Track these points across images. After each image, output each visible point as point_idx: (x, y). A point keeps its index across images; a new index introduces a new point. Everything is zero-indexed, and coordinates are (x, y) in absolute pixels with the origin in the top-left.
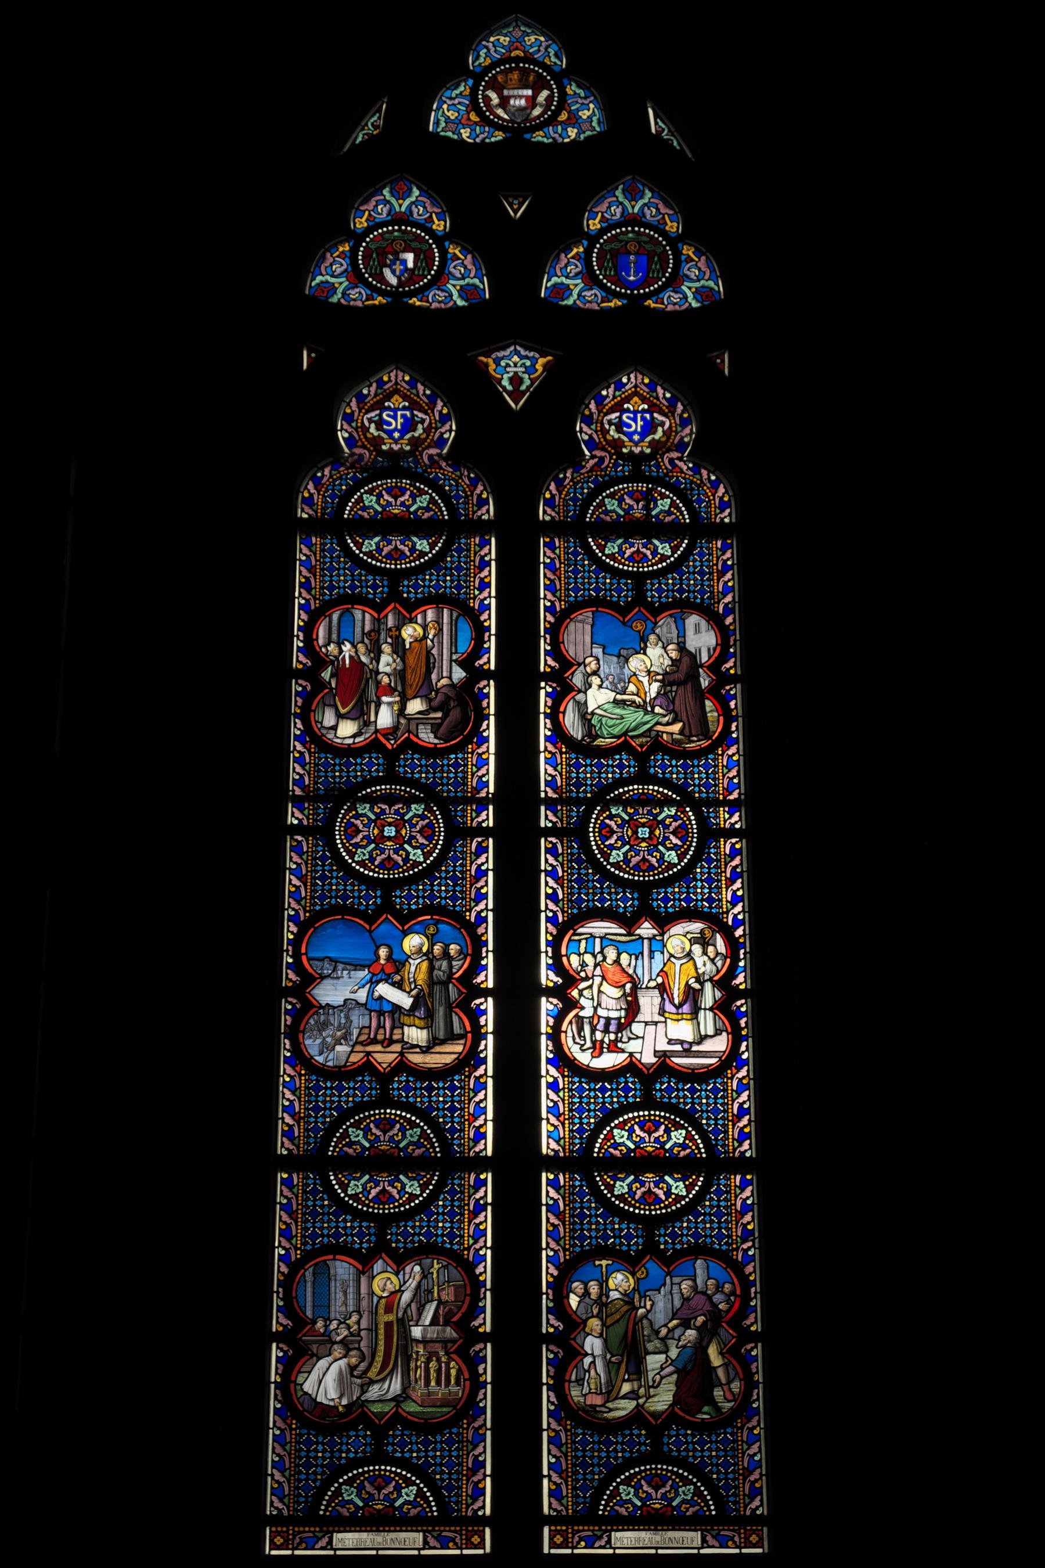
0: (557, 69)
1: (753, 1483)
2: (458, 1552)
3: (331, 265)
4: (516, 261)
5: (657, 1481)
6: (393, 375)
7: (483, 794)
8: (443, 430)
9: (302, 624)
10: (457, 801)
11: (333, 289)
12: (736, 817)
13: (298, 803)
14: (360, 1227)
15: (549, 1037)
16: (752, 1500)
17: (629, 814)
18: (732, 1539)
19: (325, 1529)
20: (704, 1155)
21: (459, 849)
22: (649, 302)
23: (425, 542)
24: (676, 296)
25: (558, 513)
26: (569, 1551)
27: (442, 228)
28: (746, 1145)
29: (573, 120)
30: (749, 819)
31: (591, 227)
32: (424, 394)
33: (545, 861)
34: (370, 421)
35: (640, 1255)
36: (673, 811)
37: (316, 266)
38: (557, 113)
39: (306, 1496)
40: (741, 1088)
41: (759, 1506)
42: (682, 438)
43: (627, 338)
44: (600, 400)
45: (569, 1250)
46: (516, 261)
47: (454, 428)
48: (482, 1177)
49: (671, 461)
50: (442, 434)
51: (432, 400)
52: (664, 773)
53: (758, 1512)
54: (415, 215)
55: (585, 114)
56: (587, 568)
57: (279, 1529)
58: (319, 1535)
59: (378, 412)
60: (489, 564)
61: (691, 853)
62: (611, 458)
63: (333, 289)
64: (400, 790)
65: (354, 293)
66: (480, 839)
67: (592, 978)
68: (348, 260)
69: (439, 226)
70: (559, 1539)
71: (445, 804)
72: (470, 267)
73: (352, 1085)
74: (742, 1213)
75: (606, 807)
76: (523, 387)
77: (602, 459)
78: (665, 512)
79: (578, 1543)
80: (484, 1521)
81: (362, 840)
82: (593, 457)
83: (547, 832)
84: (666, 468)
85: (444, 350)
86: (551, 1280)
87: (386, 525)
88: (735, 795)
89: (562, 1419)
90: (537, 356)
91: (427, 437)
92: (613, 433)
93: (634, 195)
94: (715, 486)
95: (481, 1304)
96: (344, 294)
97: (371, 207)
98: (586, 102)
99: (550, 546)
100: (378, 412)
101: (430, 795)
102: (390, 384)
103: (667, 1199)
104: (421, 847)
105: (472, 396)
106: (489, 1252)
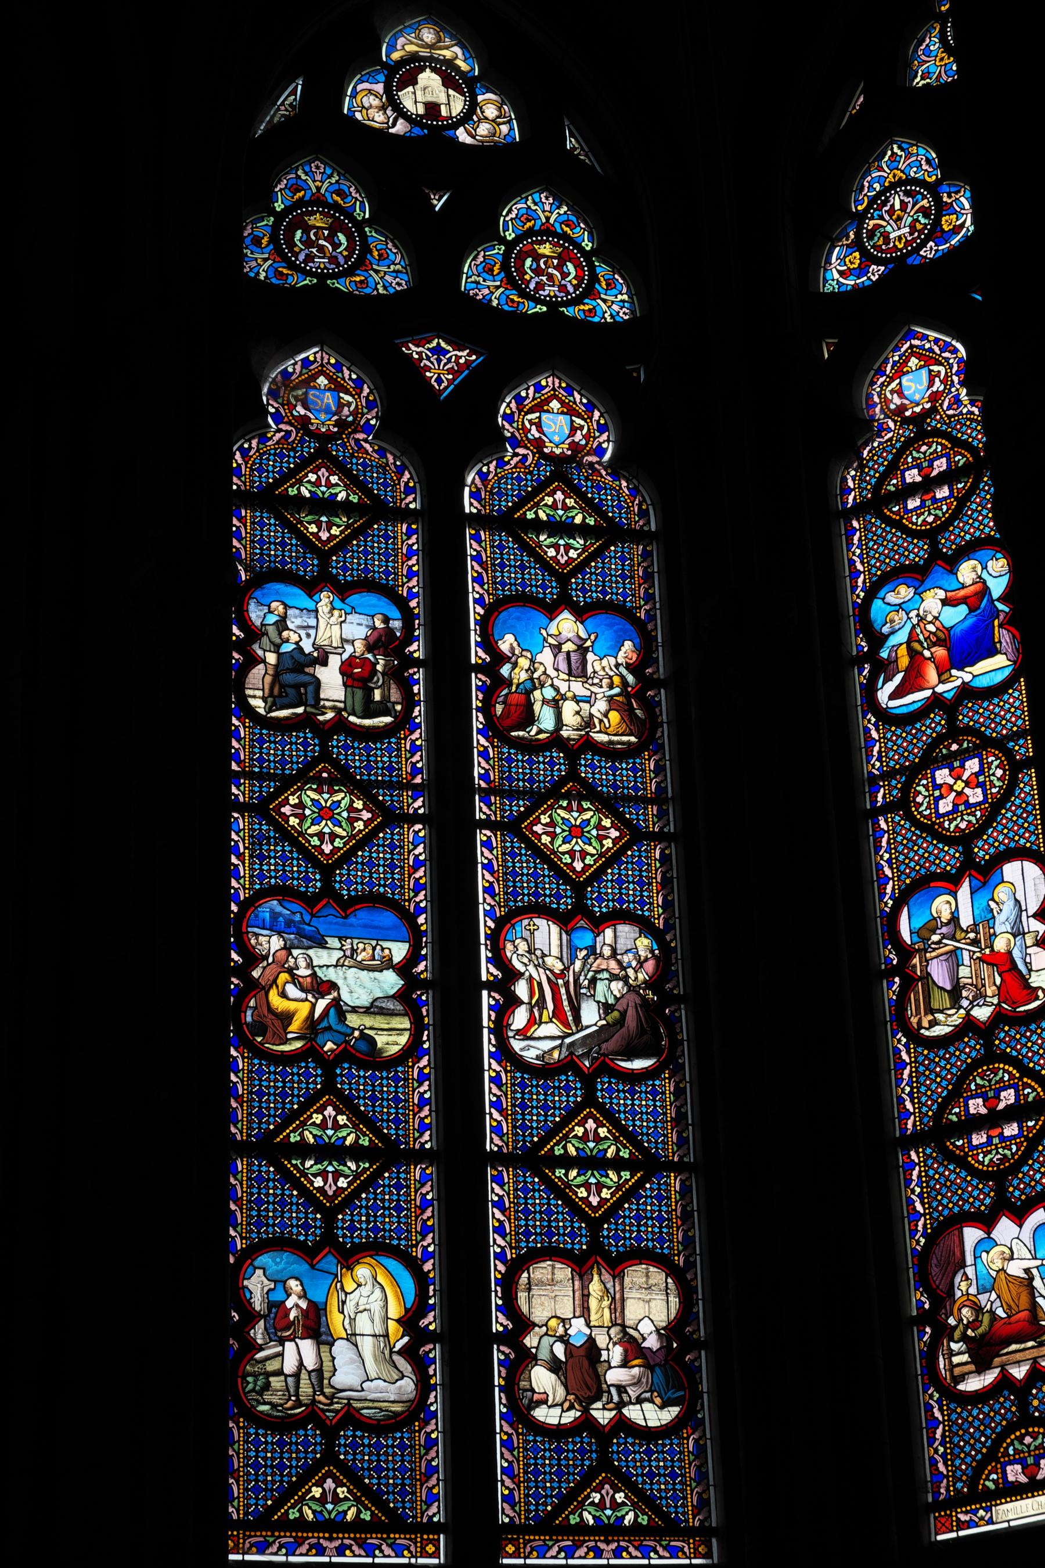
1: (430, 1489)
2: (687, 1561)
6: (550, 380)
12: (419, 803)
16: (429, 1506)
18: (408, 1549)
25: (245, 483)
26: (521, 1561)
28: (426, 1136)
30: (429, 804)
32: (350, 379)
33: (482, 855)
34: (892, 392)
40: (422, 1078)
41: (436, 1513)
42: (600, 444)
46: (436, 254)
50: (600, 444)
53: (435, 1519)
58: (550, 1543)
70: (430, 1549)
74: (423, 1208)
79: (530, 1553)
82: (279, 430)
85: (368, 334)
88: (418, 780)
92: (534, 432)
94: (400, 471)
99: (476, 538)
105: (400, 385)
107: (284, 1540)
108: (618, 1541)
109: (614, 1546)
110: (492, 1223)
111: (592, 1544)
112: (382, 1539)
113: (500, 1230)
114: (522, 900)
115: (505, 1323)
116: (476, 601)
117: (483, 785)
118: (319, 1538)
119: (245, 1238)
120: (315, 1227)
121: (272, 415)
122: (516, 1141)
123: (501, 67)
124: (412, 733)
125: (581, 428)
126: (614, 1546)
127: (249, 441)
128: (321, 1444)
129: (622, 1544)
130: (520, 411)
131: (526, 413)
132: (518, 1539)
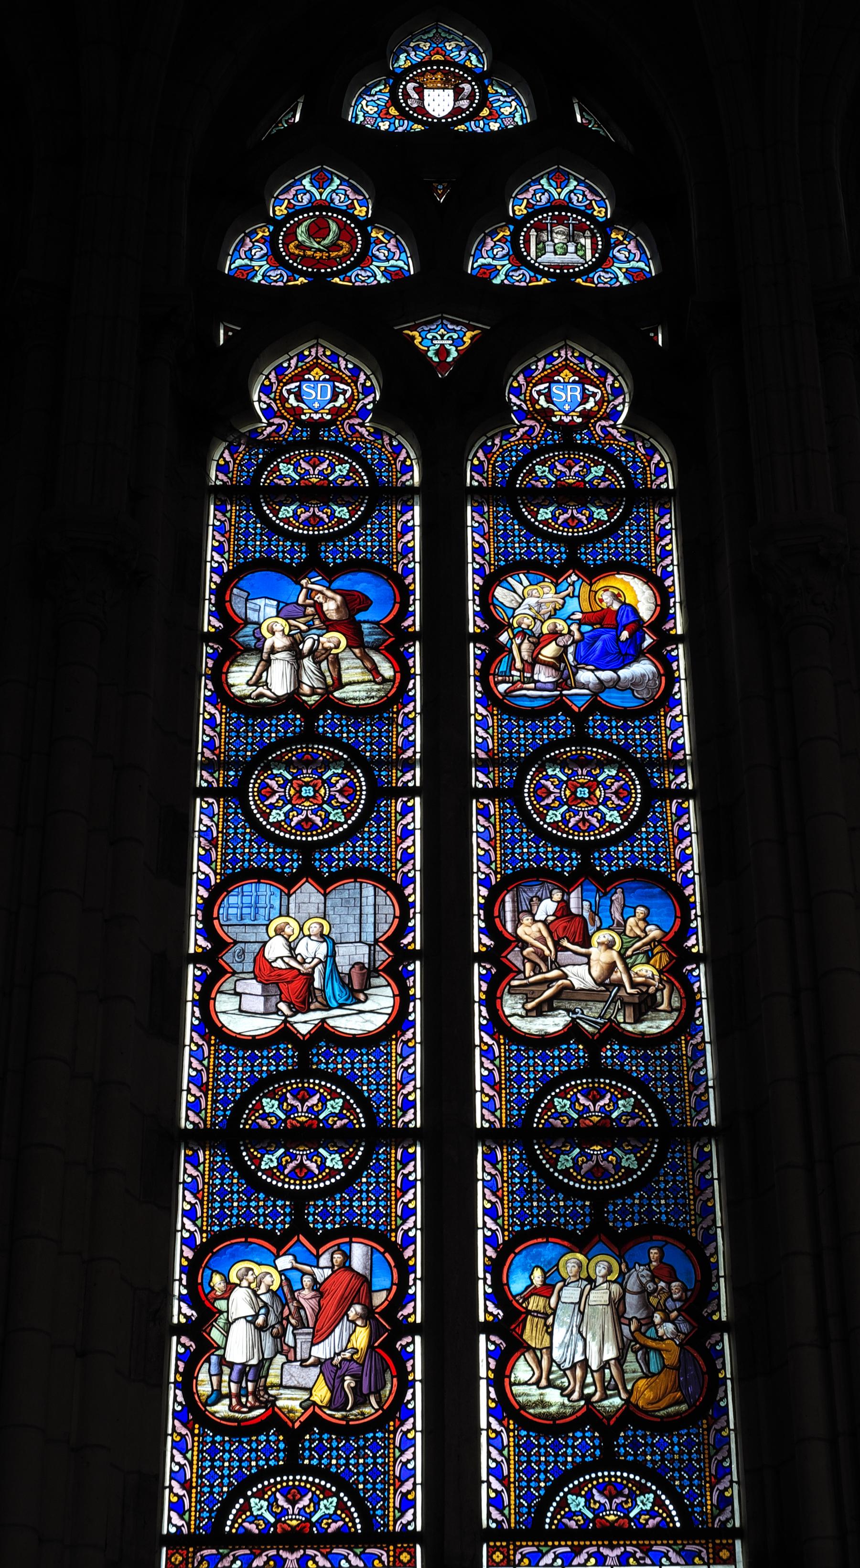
0: (478, 71)
3: (492, 248)
4: (441, 245)
5: (611, 1490)
7: (679, 756)
8: (616, 402)
9: (214, 587)
10: (652, 763)
11: (495, 270)
13: (483, 766)
14: (574, 1206)
15: (195, 1003)
17: (567, 775)
19: (550, 1543)
20: (656, 1125)
21: (659, 810)
22: (579, 280)
23: (603, 511)
24: (607, 276)
27: (364, 214)
29: (495, 115)
31: (277, 213)
34: (539, 393)
35: (287, 1236)
36: (614, 772)
37: (235, 249)
38: (479, 108)
39: (529, 1507)
43: (563, 311)
44: (528, 373)
45: (508, 1230)
46: (441, 245)
47: (627, 400)
48: (411, 1150)
49: (603, 428)
51: (603, 372)
52: (333, 733)
53: (410, 1528)
54: (337, 201)
55: (506, 111)
56: (516, 533)
57: (498, 1544)
59: (547, 385)
60: (412, 529)
61: (359, 811)
62: (289, 424)
63: (495, 270)
64: (597, 753)
65: (516, 276)
66: (405, 799)
67: (376, 941)
68: (509, 244)
69: (360, 212)
71: (640, 767)
72: (393, 249)
73: (556, 1053)
75: (267, 767)
76: (449, 359)
77: (280, 426)
78: (343, 477)
80: (735, 1533)
81: (553, 801)
82: (270, 424)
83: (479, 794)
84: (346, 434)
85: (366, 324)
86: (185, 1263)
87: (301, 493)
89: (189, 1421)
90: (465, 330)
91: (348, 408)
92: (292, 400)
93: (321, 182)
95: (714, 1289)
96: (264, 276)
97: (290, 197)
98: (508, 100)
100: (547, 385)
101: (624, 757)
102: (560, 360)
103: (320, 1173)
104: (618, 808)
106: (419, 1233)
107: (560, 1550)
108: (625, 1546)
109: (618, 1552)
110: (183, 1206)
111: (593, 1550)
112: (668, 1545)
113: (190, 1214)
114: (617, 865)
115: (495, 1311)
116: (475, 571)
117: (482, 755)
118: (598, 1546)
119: (206, 1232)
120: (314, 1214)
121: (515, 412)
122: (216, 1117)
123: (510, 63)
124: (405, 706)
125: (344, 392)
126: (618, 1552)
127: (493, 438)
128: (619, 1446)
129: (629, 1549)
130: (279, 381)
131: (535, 385)
132: (507, 1546)
